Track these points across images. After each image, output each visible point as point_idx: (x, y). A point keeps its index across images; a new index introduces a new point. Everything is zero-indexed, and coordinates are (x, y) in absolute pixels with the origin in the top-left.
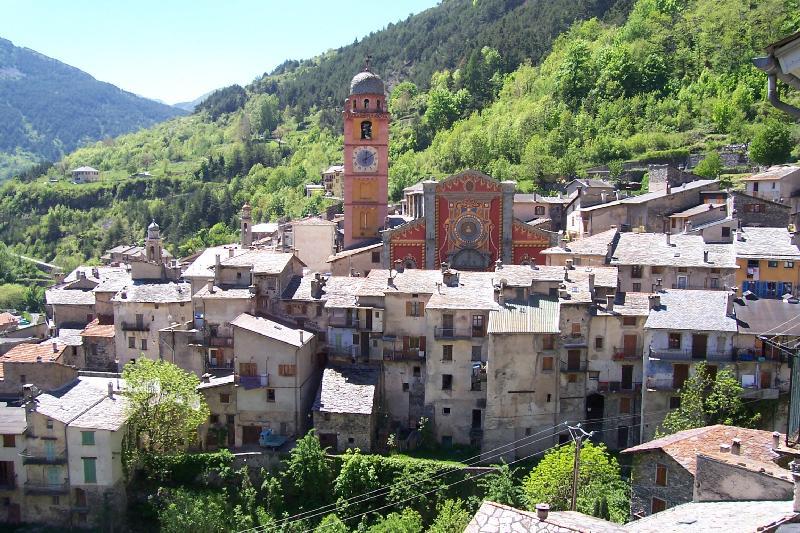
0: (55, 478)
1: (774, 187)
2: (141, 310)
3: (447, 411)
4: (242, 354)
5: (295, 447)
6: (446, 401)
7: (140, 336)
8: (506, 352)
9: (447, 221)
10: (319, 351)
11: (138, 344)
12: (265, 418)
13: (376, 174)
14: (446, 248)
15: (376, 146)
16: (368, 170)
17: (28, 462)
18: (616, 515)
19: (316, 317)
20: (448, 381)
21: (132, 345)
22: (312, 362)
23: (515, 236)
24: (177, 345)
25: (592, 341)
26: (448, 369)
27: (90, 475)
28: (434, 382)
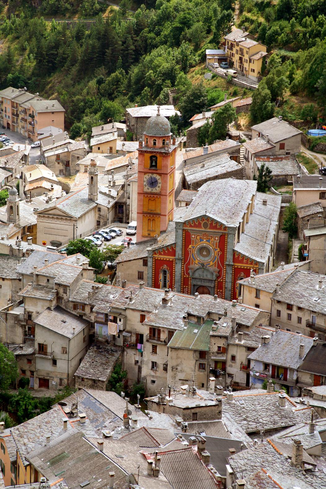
1: (84, 417)
3: (153, 382)
4: (40, 337)
6: (153, 376)
8: (178, 358)
9: (190, 246)
10: (91, 333)
12: (51, 375)
13: (160, 194)
14: (189, 264)
15: (160, 174)
16: (154, 191)
19: (90, 314)
20: (154, 364)
22: (84, 341)
23: (234, 260)
24: (8, 321)
25: (229, 357)
26: (155, 358)
28: (147, 364)
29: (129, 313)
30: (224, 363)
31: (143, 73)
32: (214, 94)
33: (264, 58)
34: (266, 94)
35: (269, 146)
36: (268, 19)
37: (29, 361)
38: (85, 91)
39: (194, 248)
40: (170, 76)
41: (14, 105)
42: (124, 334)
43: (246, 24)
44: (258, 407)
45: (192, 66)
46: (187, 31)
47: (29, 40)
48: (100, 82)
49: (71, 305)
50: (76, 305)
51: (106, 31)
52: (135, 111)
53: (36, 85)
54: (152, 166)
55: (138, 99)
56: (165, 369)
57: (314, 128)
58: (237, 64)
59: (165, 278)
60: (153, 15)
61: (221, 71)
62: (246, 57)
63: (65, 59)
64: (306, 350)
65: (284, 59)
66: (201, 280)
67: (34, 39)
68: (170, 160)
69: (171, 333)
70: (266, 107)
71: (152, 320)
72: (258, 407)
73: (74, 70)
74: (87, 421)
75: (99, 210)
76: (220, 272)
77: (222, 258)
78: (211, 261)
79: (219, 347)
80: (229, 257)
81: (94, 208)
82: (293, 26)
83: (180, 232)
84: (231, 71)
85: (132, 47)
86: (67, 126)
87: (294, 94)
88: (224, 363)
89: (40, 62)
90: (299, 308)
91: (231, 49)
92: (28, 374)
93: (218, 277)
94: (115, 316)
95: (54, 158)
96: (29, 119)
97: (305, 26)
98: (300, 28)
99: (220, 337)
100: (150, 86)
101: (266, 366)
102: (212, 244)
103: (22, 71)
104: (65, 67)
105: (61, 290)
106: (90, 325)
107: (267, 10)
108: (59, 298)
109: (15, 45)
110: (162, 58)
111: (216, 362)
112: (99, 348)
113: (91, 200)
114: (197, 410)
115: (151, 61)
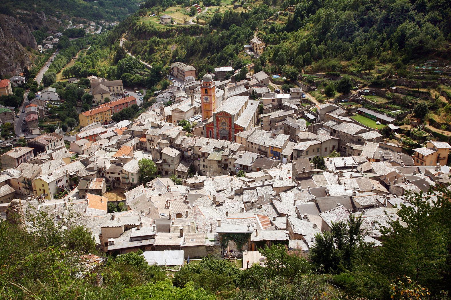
0: (127, 181)
2: (152, 136)
4: (164, 157)
5: (436, 17)
7: (152, 143)
11: (152, 144)
13: (209, 103)
15: (209, 96)
16: (207, 102)
17: (123, 178)
18: (422, 145)
20: (204, 166)
21: (150, 144)
25: (229, 162)
26: (204, 163)
27: (133, 181)
29: (195, 147)
30: (227, 165)
31: (222, 55)
32: (246, 62)
33: (264, 48)
34: (259, 63)
35: (258, 82)
36: (266, 34)
37: (161, 165)
38: (203, 62)
39: (220, 123)
40: (231, 55)
41: (178, 69)
42: (194, 155)
43: (259, 35)
44: (223, 182)
45: (240, 51)
46: (238, 38)
47: (184, 44)
48: (208, 58)
49: (175, 145)
50: (177, 145)
51: (210, 40)
52: (218, 70)
53: (186, 61)
54: (206, 93)
55: (220, 65)
56: (207, 167)
57: (275, 75)
58: (255, 51)
59: (211, 134)
60: (228, 33)
61: (249, 53)
62: (258, 48)
63: (196, 50)
64: (255, 159)
65: (271, 48)
66: (223, 134)
67: (186, 44)
68: (212, 90)
69: (209, 154)
70: (259, 67)
71: (203, 150)
72: (223, 182)
73: (199, 54)
74: (155, 189)
75: (195, 108)
76: (230, 131)
77: (230, 126)
78: (226, 127)
79: (225, 159)
80: (233, 125)
81: (193, 108)
82: (275, 36)
83: (215, 117)
84: (253, 53)
85: (220, 45)
86: (197, 75)
87: (270, 62)
88: (227, 165)
89: (188, 53)
90: (255, 144)
91: (253, 45)
92: (161, 170)
93: (229, 133)
94: (191, 148)
95: (188, 88)
96: (183, 73)
97: (279, 36)
98: (278, 36)
99: (225, 155)
100: (225, 59)
101: (241, 165)
102: (226, 121)
103: (181, 56)
104: (196, 54)
105: (172, 140)
106: (182, 152)
107: (266, 30)
108: (171, 142)
109: (180, 46)
110: (229, 48)
111: (224, 164)
112: (185, 160)
113: (192, 105)
114: (195, 184)
115: (225, 50)
